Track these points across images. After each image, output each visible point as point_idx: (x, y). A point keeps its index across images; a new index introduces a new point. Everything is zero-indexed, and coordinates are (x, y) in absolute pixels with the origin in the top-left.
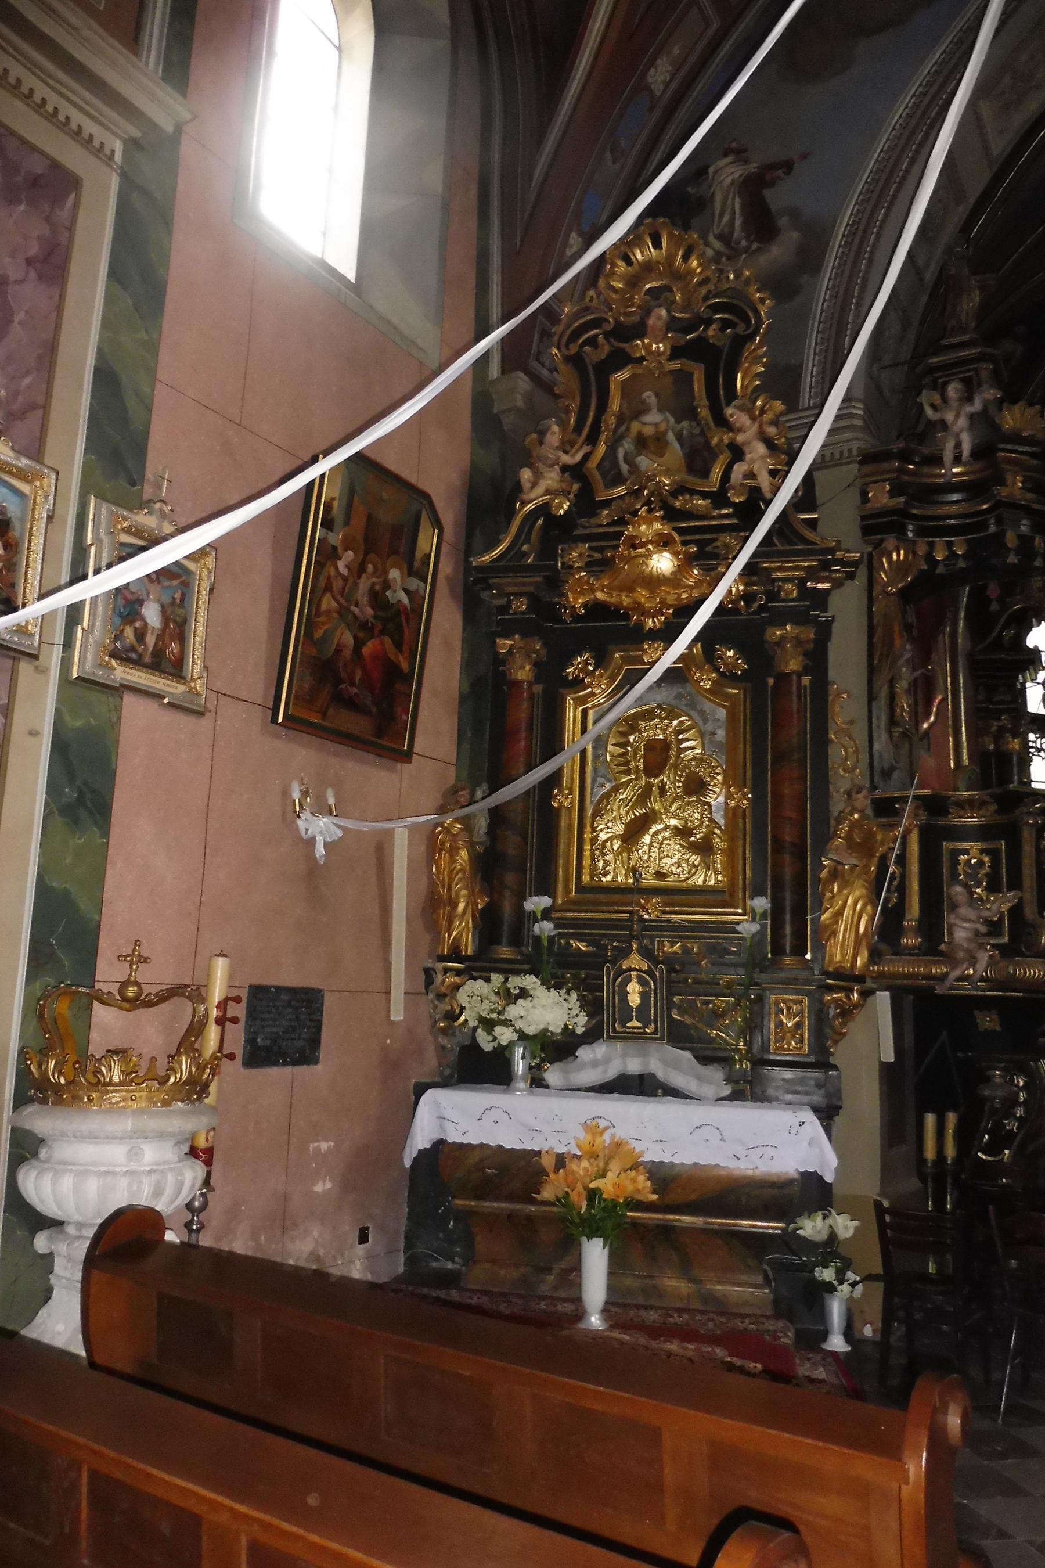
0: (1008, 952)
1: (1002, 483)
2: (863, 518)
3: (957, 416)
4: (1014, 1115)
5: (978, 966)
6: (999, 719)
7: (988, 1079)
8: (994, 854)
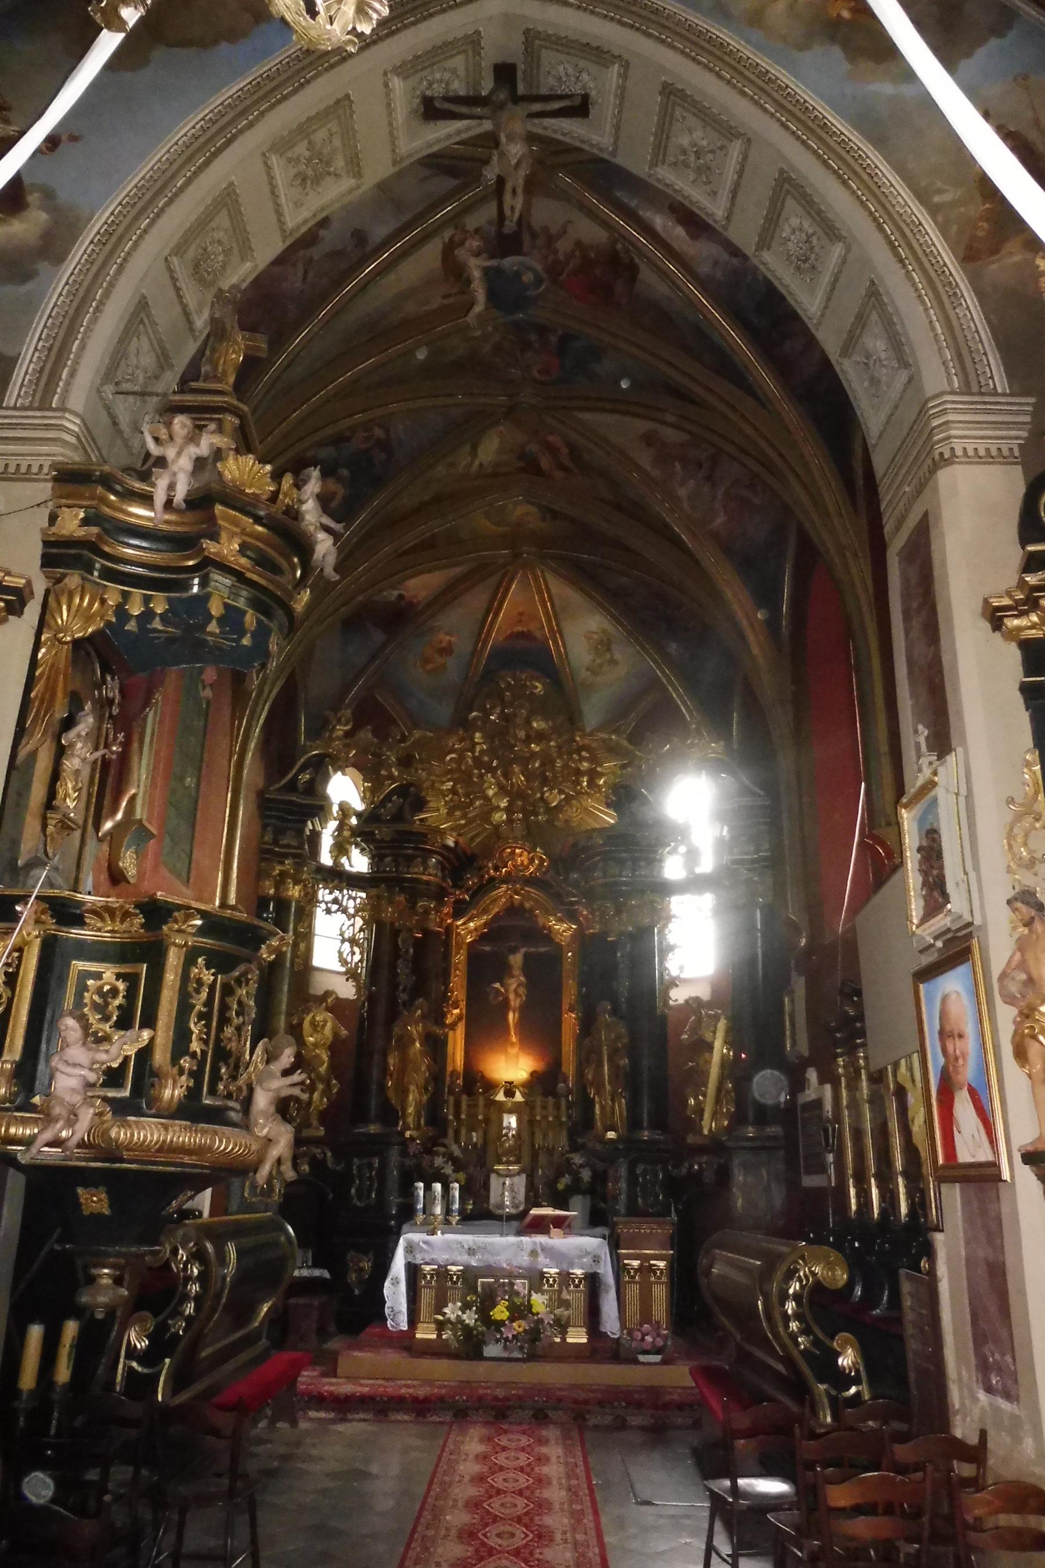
0: (122, 1109)
1: (214, 537)
2: (46, 544)
3: (179, 454)
4: (181, 1314)
5: (77, 1127)
6: (282, 863)
7: (92, 1280)
8: (132, 979)
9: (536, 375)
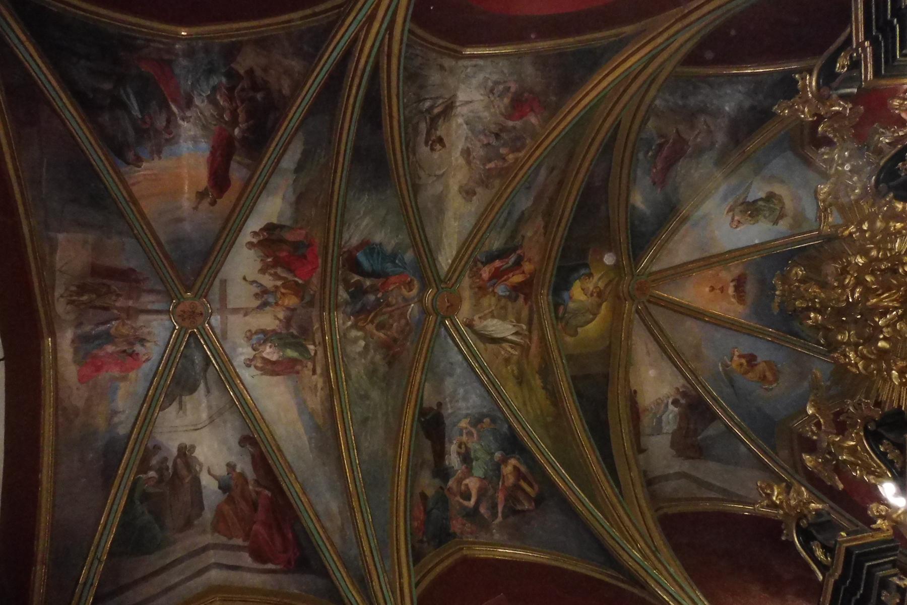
9: (415, 291)
